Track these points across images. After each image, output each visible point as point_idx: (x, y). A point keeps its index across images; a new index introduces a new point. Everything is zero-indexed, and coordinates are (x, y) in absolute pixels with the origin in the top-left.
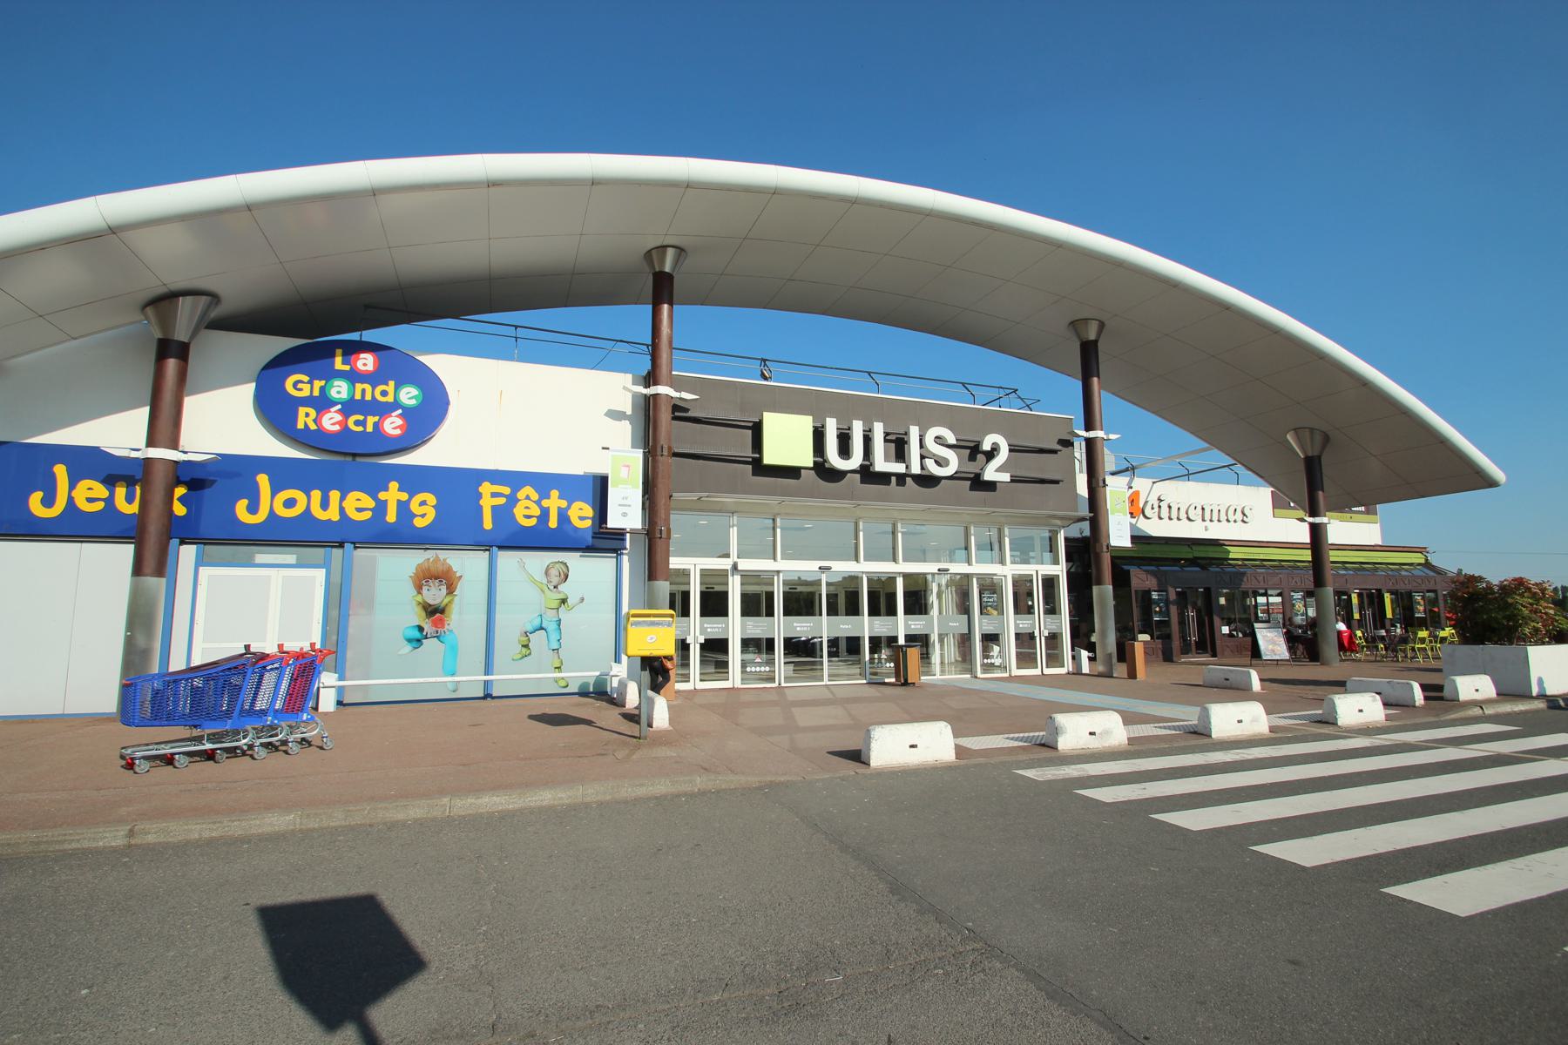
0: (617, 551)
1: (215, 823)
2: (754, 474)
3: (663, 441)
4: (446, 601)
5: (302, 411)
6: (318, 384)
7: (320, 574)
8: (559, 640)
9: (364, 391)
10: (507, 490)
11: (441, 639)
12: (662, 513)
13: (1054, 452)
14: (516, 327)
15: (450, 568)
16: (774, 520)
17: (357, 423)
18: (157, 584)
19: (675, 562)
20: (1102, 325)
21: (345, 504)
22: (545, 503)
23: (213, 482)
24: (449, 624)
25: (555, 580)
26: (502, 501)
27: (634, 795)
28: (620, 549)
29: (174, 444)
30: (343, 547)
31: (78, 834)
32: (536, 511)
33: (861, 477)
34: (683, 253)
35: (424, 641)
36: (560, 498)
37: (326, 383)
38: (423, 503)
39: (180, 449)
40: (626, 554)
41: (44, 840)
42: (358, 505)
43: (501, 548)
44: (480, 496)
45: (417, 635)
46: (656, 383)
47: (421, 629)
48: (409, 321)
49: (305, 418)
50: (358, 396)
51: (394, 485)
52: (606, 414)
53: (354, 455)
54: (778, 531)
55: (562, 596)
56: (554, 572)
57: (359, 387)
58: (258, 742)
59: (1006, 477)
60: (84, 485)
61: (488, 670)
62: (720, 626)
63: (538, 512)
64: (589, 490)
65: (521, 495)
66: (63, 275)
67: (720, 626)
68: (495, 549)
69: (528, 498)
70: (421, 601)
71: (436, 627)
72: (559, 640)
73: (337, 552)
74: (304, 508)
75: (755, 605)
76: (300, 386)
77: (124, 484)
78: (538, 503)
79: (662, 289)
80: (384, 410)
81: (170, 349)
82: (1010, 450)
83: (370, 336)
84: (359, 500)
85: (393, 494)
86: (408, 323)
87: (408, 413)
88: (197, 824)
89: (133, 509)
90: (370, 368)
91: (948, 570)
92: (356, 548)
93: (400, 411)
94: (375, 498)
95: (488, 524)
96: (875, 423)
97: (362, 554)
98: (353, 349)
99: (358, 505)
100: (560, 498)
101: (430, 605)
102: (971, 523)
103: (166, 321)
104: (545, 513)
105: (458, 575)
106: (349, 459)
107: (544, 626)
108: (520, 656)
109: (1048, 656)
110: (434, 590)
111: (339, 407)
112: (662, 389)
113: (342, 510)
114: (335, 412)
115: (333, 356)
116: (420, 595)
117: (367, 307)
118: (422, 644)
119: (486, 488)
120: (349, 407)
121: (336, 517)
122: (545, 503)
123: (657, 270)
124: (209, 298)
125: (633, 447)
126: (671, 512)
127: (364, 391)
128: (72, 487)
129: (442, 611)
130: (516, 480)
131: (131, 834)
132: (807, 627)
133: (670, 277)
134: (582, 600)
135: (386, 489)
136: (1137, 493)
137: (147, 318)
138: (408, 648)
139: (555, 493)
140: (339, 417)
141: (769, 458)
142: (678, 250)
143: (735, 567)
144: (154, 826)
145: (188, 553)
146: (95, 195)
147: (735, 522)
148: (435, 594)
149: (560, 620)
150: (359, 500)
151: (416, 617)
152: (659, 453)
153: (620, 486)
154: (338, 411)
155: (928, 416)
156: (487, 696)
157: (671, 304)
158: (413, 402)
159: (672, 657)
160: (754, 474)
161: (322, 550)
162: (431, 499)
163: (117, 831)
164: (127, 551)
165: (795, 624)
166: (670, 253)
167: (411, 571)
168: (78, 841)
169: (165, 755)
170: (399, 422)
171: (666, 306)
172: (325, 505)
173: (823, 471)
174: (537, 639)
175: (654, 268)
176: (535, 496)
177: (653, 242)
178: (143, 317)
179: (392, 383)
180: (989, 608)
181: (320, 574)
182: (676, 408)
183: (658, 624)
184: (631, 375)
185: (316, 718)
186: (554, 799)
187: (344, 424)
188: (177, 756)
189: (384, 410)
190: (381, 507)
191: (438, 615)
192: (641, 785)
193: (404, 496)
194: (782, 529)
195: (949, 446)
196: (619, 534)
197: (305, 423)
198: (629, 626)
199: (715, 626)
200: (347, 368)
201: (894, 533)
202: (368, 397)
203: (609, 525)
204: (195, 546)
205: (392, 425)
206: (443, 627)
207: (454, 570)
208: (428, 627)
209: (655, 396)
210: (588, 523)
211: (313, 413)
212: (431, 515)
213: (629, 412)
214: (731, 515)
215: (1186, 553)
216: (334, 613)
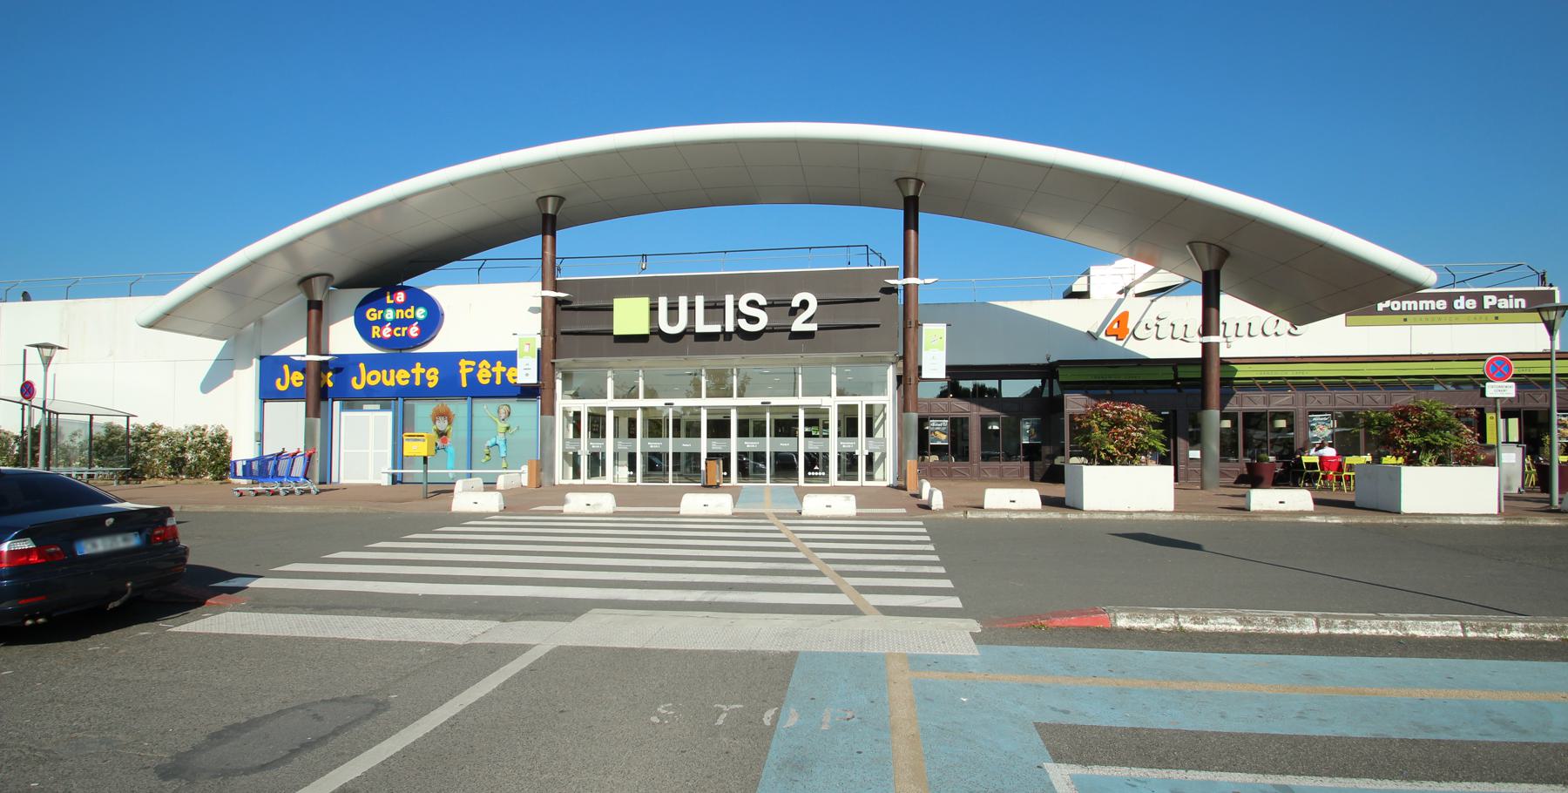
5: (374, 328)
6: (381, 312)
10: (473, 363)
13: (878, 300)
15: (449, 410)
20: (919, 182)
22: (494, 370)
26: (472, 369)
38: (432, 374)
42: (401, 377)
44: (460, 367)
51: (418, 365)
52: (529, 310)
56: (502, 411)
57: (398, 311)
59: (813, 327)
63: (490, 375)
65: (481, 366)
69: (484, 367)
75: (719, 428)
78: (490, 370)
79: (549, 225)
81: (315, 306)
82: (819, 304)
85: (418, 370)
87: (421, 324)
90: (402, 300)
91: (672, 404)
94: (410, 372)
95: (464, 384)
99: (401, 377)
109: (867, 476)
113: (396, 380)
119: (463, 363)
120: (396, 323)
121: (393, 384)
122: (494, 370)
127: (400, 314)
128: (290, 375)
129: (446, 434)
130: (477, 357)
131: (181, 508)
135: (415, 367)
136: (1125, 315)
139: (499, 363)
140: (390, 330)
148: (442, 424)
154: (417, 326)
155: (739, 284)
158: (423, 317)
166: (550, 200)
170: (417, 329)
173: (655, 331)
176: (489, 366)
179: (413, 307)
180: (937, 432)
183: (419, 440)
187: (392, 333)
189: (408, 323)
190: (413, 376)
195: (762, 308)
200: (392, 302)
205: (414, 331)
211: (378, 328)
215: (1167, 374)
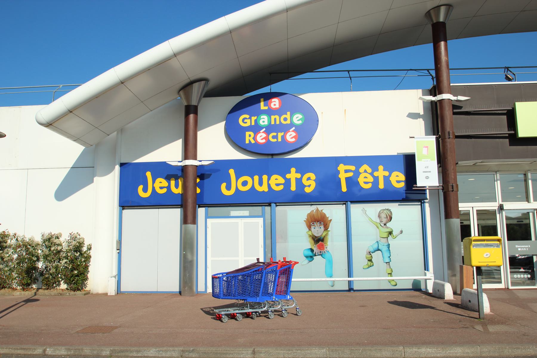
0: (421, 202)
1: (289, 350)
2: (510, 145)
3: (448, 128)
4: (324, 234)
5: (247, 134)
6: (254, 118)
7: (260, 221)
8: (389, 257)
9: (275, 119)
10: (353, 168)
11: (323, 256)
12: (451, 176)
14: (348, 71)
16: (525, 174)
17: (273, 137)
18: (191, 226)
19: (463, 206)
21: (270, 182)
22: (376, 174)
23: (210, 175)
24: (326, 248)
25: (385, 220)
26: (350, 174)
27: (513, 354)
28: (423, 200)
29: (195, 158)
30: (271, 206)
31: (232, 350)
33: (509, 140)
34: (451, 7)
35: (314, 257)
36: (296, 172)
37: (257, 118)
38: (309, 179)
39: (198, 159)
40: (427, 202)
41: (219, 352)
43: (352, 202)
44: (338, 172)
45: (310, 253)
46: (441, 93)
47: (312, 250)
48: (287, 78)
49: (249, 137)
50: (273, 123)
51: (293, 170)
52: (408, 116)
53: (272, 155)
54: (530, 182)
55: (389, 230)
57: (273, 117)
58: (270, 310)
60: (159, 180)
61: (350, 275)
62: (527, 246)
64: (402, 164)
65: (361, 170)
66: (145, 81)
67: (527, 246)
68: (349, 203)
69: (365, 171)
70: (311, 234)
71: (320, 249)
72: (389, 257)
73: (268, 209)
74: (251, 186)
76: (245, 121)
77: (174, 179)
78: (372, 174)
80: (285, 128)
83: (275, 88)
84: (161, 182)
85: (293, 175)
86: (287, 79)
87: (298, 129)
88: (281, 350)
89: (178, 191)
92: (277, 206)
93: (294, 128)
94: (284, 177)
95: (344, 189)
96: (516, 103)
97: (280, 209)
98: (268, 97)
100: (296, 172)
101: (316, 237)
102: (529, 170)
103: (188, 97)
104: (376, 179)
105: (329, 219)
106: (270, 157)
107: (380, 248)
108: (367, 266)
110: (317, 228)
111: (264, 129)
112: (445, 96)
113: (269, 185)
114: (292, 131)
115: (260, 102)
116: (310, 231)
117: (270, 74)
118: (313, 259)
119: (342, 168)
120: (269, 129)
121: (266, 190)
122: (376, 174)
123: (435, 21)
124: (204, 82)
125: (426, 135)
126: (457, 174)
127: (275, 119)
128: (154, 182)
132: (526, 248)
133: (443, 24)
134: (401, 232)
135: (384, 170)
137: (180, 96)
138: (306, 261)
139: (381, 168)
140: (264, 135)
141: (523, 132)
142: (447, 7)
143: (501, 208)
144: (263, 349)
145: (201, 212)
146: (168, 40)
147: (498, 178)
148: (318, 231)
149: (389, 245)
150: (161, 182)
151: (308, 244)
152: (447, 136)
153: (423, 160)
156: (350, 290)
157: (446, 40)
158: (300, 122)
159: (498, 269)
160: (510, 145)
161: (260, 208)
162: (312, 176)
163: (248, 350)
164: (177, 213)
165: (517, 246)
166: (443, 10)
167: (305, 217)
168: (232, 354)
169: (231, 314)
170: (294, 134)
171: (442, 43)
172: (261, 183)
174: (376, 256)
175: (432, 20)
176: (369, 170)
177: (430, 5)
178: (178, 96)
179: (289, 113)
181: (260, 221)
182: (454, 107)
184: (421, 90)
185: (293, 298)
186: (464, 353)
187: (267, 138)
188: (238, 315)
189: (285, 128)
190: (288, 182)
191: (320, 242)
192: (518, 348)
193: (299, 176)
194: (532, 180)
196: (422, 191)
197: (249, 140)
198: (472, 247)
199: (523, 246)
200: (266, 108)
201: (526, 181)
202: (278, 123)
203: (418, 185)
204: (204, 208)
205: (291, 137)
206: (323, 249)
207: (327, 216)
208: (316, 250)
209: (441, 101)
210: (402, 185)
211: (252, 134)
212: (313, 185)
213: (422, 113)
214: (495, 173)
216: (268, 242)
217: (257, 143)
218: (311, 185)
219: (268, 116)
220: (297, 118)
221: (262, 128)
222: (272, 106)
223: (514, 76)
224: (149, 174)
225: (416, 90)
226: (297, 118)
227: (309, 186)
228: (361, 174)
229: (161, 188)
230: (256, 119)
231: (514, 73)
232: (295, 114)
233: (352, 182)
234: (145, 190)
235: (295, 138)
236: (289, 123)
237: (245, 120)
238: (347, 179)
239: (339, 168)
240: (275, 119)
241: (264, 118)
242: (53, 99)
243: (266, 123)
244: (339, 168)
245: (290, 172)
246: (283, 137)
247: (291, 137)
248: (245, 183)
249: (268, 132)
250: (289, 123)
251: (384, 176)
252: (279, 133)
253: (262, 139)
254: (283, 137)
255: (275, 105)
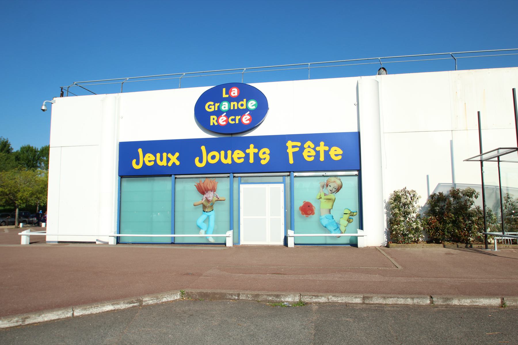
5: (212, 117)
6: (217, 105)
7: (282, 186)
10: (299, 144)
17: (232, 120)
21: (233, 156)
22: (318, 149)
26: (297, 149)
32: (313, 153)
37: (220, 104)
38: (264, 153)
49: (213, 120)
50: (232, 108)
51: (252, 146)
57: (232, 103)
65: (306, 146)
69: (309, 147)
76: (210, 107)
78: (314, 149)
80: (241, 112)
84: (238, 154)
85: (252, 150)
87: (253, 113)
93: (249, 112)
94: (244, 152)
95: (291, 161)
100: (325, 145)
104: (318, 153)
111: (225, 114)
113: (232, 159)
119: (290, 144)
120: (230, 113)
122: (318, 149)
128: (144, 157)
139: (322, 143)
140: (225, 118)
150: (238, 154)
158: (254, 108)
162: (267, 151)
170: (248, 117)
172: (226, 157)
176: (312, 146)
179: (245, 100)
181: (282, 186)
187: (227, 121)
189: (241, 112)
190: (247, 156)
193: (256, 151)
197: (213, 123)
200: (227, 96)
202: (236, 108)
205: (246, 119)
212: (268, 158)
217: (219, 125)
218: (265, 158)
219: (228, 103)
220: (251, 104)
221: (223, 113)
222: (232, 94)
223: (455, 61)
224: (140, 151)
225: (360, 77)
226: (251, 104)
227: (265, 159)
228: (305, 149)
229: (150, 161)
230: (219, 105)
231: (455, 58)
232: (249, 101)
233: (298, 155)
234: (138, 163)
235: (249, 121)
236: (245, 108)
237: (210, 106)
238: (294, 153)
239: (287, 144)
240: (234, 105)
241: (225, 105)
242: (180, 84)
243: (227, 109)
244: (287, 144)
245: (249, 148)
246: (240, 120)
247: (246, 119)
248: (213, 157)
249: (228, 116)
250: (245, 108)
251: (325, 151)
252: (236, 117)
253: (247, 120)
254: (240, 120)
255: (234, 93)
